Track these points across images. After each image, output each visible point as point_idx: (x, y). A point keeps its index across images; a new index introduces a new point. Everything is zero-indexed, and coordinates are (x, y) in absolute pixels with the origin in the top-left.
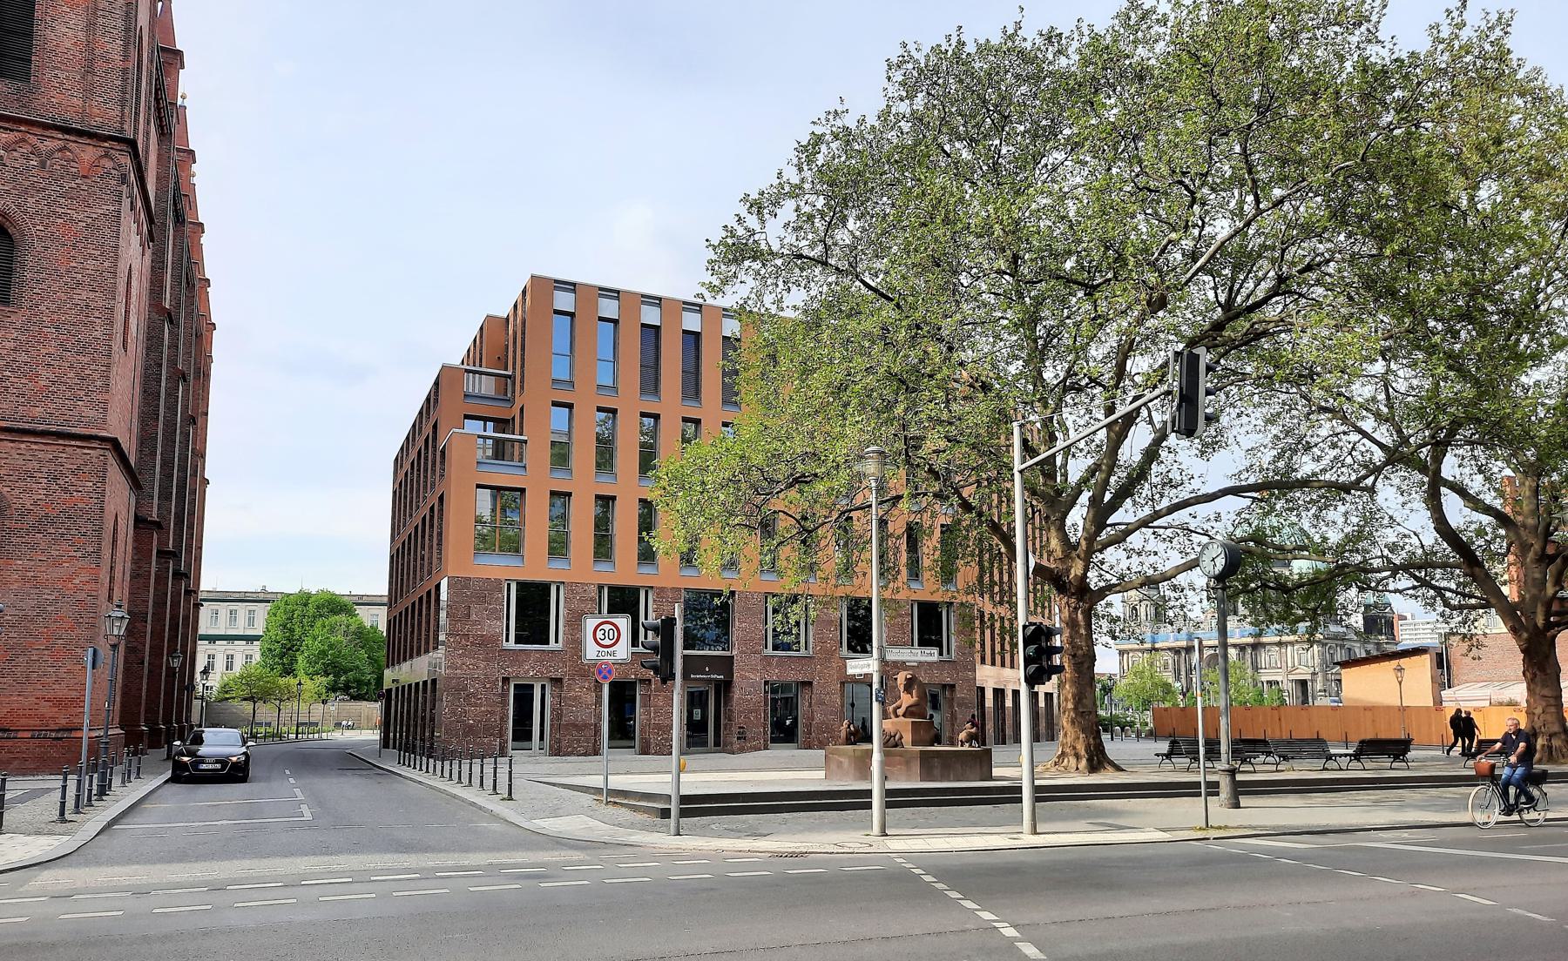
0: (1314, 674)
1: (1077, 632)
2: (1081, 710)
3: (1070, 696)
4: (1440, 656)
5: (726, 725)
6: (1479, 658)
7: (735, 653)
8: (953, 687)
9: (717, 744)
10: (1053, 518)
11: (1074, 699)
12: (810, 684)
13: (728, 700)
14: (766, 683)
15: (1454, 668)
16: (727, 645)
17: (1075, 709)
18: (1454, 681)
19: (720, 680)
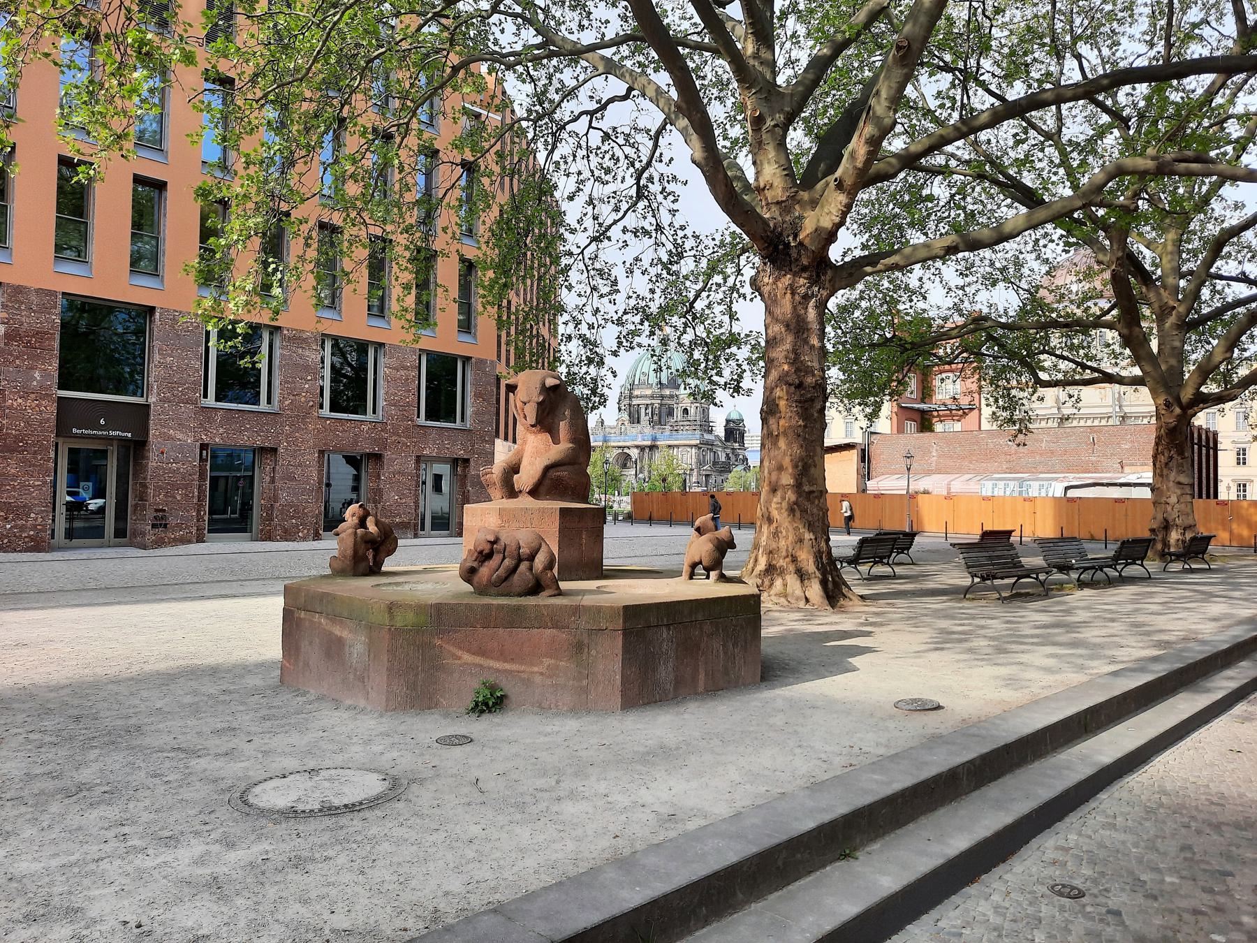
0: (691, 470)
1: (806, 341)
2: (806, 488)
3: (787, 462)
4: (863, 451)
5: (136, 506)
6: (1025, 445)
7: (152, 399)
8: (467, 461)
9: (120, 533)
10: (769, 123)
11: (795, 466)
12: (274, 450)
13: (140, 467)
14: (203, 447)
15: (873, 462)
16: (138, 389)
17: (798, 486)
18: (873, 473)
19: (126, 440)
